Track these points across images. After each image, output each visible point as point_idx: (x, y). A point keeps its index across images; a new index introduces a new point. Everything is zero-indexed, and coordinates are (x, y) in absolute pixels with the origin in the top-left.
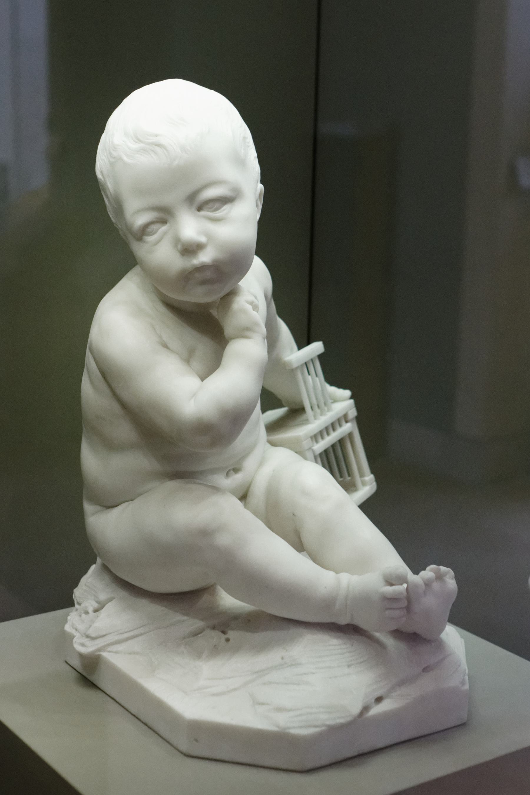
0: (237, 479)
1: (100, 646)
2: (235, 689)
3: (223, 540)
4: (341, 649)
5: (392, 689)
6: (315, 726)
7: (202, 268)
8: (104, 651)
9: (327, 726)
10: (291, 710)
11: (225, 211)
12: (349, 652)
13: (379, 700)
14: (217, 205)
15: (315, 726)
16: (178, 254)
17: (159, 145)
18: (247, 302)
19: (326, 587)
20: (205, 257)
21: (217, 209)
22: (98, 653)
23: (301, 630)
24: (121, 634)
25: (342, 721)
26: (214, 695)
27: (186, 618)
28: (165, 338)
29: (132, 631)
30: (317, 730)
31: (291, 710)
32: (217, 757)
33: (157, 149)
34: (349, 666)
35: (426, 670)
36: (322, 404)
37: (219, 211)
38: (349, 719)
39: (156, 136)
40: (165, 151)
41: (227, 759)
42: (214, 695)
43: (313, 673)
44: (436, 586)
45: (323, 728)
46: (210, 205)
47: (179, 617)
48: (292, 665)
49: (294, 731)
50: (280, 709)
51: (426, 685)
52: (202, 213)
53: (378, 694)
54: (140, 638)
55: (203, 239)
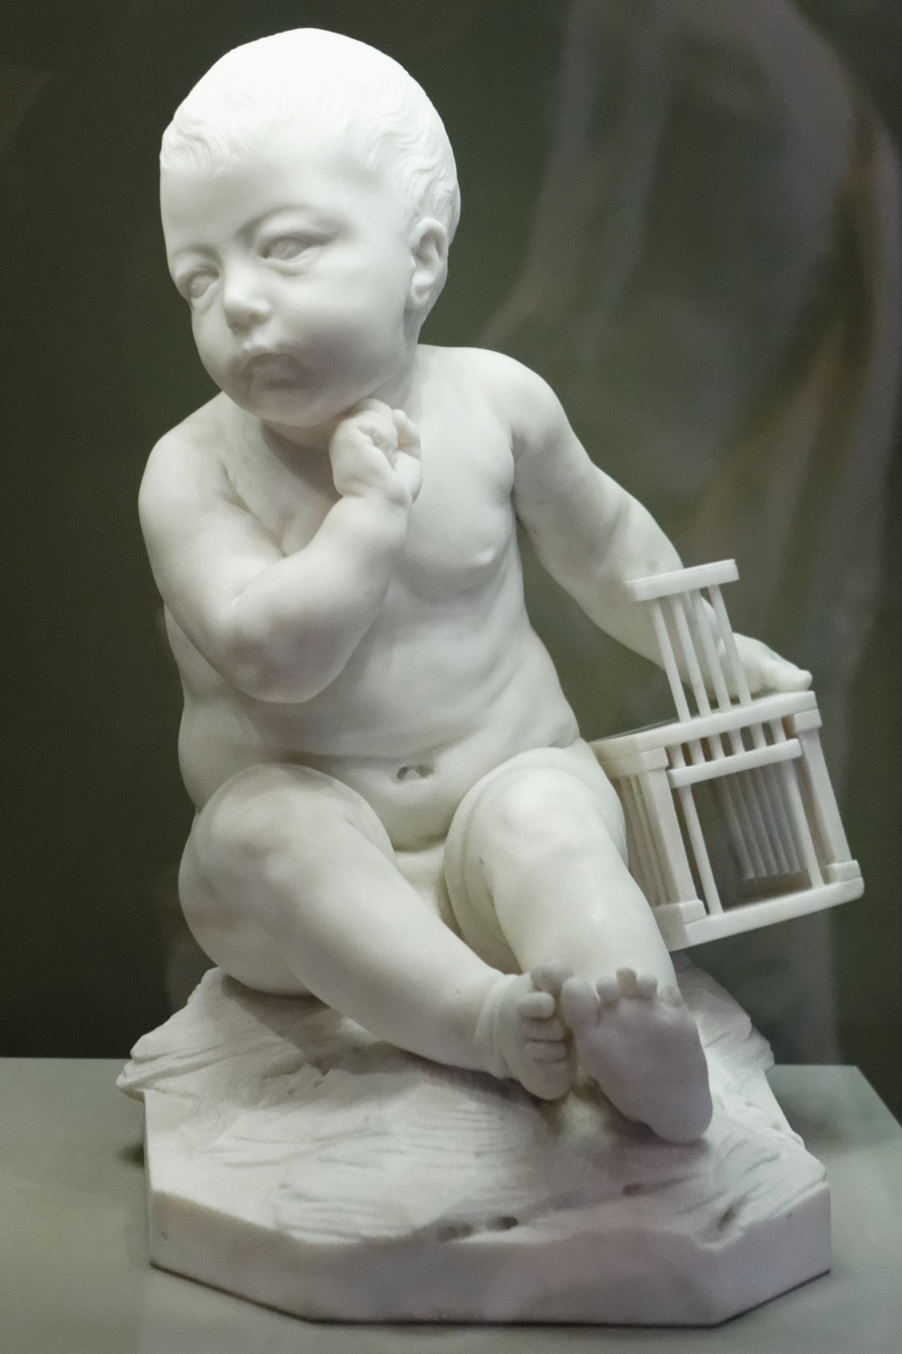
0: (417, 789)
1: (143, 1075)
2: (270, 1163)
3: (279, 869)
4: (475, 1121)
5: (541, 1208)
6: (340, 1234)
7: (262, 358)
8: (150, 1088)
9: (364, 1238)
10: (316, 1200)
11: (308, 256)
12: (489, 1129)
13: (508, 1223)
14: (291, 248)
15: (340, 1234)
16: (229, 331)
17: (200, 139)
18: (371, 432)
19: (458, 992)
20: (264, 339)
21: (291, 255)
22: (140, 1090)
23: (415, 1074)
24: (182, 1058)
25: (391, 1234)
26: (231, 1165)
27: (279, 1039)
28: (241, 490)
29: (198, 1054)
30: (334, 1240)
31: (316, 1200)
32: (191, 1273)
33: (197, 145)
34: (478, 1154)
35: (630, 1191)
36: (723, 695)
37: (292, 260)
38: (403, 1232)
39: (198, 123)
40: (206, 150)
41: (203, 1276)
42: (231, 1165)
43: (401, 1152)
44: (627, 1008)
45: (354, 1241)
46: (280, 247)
47: (270, 1037)
48: (377, 1134)
49: (297, 1235)
50: (299, 1196)
51: (615, 1217)
52: (272, 260)
53: (510, 1209)
54: (204, 1071)
55: (261, 306)
